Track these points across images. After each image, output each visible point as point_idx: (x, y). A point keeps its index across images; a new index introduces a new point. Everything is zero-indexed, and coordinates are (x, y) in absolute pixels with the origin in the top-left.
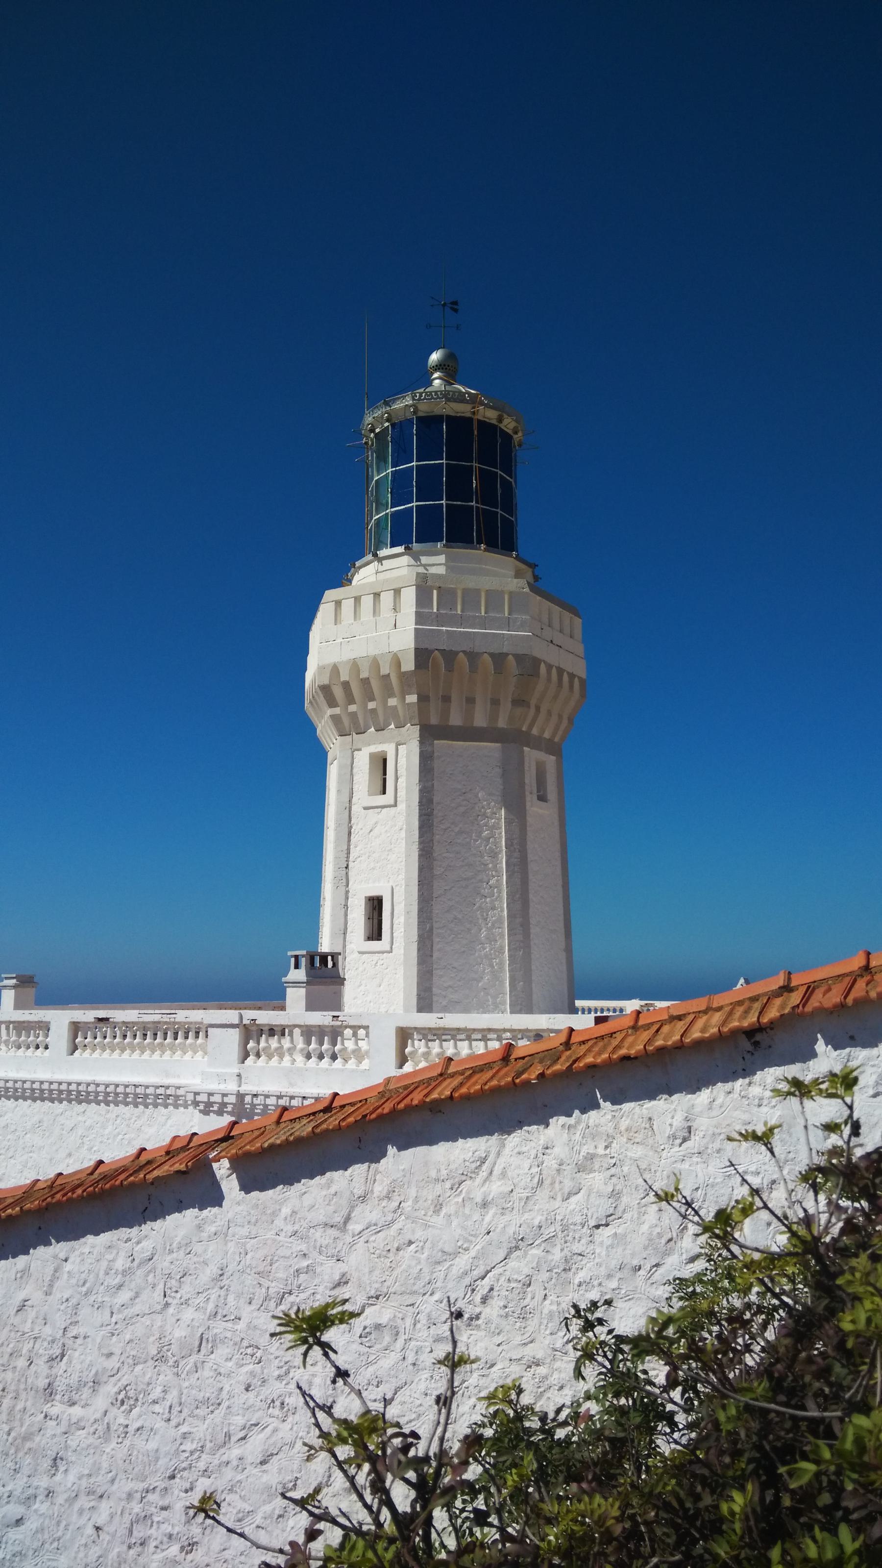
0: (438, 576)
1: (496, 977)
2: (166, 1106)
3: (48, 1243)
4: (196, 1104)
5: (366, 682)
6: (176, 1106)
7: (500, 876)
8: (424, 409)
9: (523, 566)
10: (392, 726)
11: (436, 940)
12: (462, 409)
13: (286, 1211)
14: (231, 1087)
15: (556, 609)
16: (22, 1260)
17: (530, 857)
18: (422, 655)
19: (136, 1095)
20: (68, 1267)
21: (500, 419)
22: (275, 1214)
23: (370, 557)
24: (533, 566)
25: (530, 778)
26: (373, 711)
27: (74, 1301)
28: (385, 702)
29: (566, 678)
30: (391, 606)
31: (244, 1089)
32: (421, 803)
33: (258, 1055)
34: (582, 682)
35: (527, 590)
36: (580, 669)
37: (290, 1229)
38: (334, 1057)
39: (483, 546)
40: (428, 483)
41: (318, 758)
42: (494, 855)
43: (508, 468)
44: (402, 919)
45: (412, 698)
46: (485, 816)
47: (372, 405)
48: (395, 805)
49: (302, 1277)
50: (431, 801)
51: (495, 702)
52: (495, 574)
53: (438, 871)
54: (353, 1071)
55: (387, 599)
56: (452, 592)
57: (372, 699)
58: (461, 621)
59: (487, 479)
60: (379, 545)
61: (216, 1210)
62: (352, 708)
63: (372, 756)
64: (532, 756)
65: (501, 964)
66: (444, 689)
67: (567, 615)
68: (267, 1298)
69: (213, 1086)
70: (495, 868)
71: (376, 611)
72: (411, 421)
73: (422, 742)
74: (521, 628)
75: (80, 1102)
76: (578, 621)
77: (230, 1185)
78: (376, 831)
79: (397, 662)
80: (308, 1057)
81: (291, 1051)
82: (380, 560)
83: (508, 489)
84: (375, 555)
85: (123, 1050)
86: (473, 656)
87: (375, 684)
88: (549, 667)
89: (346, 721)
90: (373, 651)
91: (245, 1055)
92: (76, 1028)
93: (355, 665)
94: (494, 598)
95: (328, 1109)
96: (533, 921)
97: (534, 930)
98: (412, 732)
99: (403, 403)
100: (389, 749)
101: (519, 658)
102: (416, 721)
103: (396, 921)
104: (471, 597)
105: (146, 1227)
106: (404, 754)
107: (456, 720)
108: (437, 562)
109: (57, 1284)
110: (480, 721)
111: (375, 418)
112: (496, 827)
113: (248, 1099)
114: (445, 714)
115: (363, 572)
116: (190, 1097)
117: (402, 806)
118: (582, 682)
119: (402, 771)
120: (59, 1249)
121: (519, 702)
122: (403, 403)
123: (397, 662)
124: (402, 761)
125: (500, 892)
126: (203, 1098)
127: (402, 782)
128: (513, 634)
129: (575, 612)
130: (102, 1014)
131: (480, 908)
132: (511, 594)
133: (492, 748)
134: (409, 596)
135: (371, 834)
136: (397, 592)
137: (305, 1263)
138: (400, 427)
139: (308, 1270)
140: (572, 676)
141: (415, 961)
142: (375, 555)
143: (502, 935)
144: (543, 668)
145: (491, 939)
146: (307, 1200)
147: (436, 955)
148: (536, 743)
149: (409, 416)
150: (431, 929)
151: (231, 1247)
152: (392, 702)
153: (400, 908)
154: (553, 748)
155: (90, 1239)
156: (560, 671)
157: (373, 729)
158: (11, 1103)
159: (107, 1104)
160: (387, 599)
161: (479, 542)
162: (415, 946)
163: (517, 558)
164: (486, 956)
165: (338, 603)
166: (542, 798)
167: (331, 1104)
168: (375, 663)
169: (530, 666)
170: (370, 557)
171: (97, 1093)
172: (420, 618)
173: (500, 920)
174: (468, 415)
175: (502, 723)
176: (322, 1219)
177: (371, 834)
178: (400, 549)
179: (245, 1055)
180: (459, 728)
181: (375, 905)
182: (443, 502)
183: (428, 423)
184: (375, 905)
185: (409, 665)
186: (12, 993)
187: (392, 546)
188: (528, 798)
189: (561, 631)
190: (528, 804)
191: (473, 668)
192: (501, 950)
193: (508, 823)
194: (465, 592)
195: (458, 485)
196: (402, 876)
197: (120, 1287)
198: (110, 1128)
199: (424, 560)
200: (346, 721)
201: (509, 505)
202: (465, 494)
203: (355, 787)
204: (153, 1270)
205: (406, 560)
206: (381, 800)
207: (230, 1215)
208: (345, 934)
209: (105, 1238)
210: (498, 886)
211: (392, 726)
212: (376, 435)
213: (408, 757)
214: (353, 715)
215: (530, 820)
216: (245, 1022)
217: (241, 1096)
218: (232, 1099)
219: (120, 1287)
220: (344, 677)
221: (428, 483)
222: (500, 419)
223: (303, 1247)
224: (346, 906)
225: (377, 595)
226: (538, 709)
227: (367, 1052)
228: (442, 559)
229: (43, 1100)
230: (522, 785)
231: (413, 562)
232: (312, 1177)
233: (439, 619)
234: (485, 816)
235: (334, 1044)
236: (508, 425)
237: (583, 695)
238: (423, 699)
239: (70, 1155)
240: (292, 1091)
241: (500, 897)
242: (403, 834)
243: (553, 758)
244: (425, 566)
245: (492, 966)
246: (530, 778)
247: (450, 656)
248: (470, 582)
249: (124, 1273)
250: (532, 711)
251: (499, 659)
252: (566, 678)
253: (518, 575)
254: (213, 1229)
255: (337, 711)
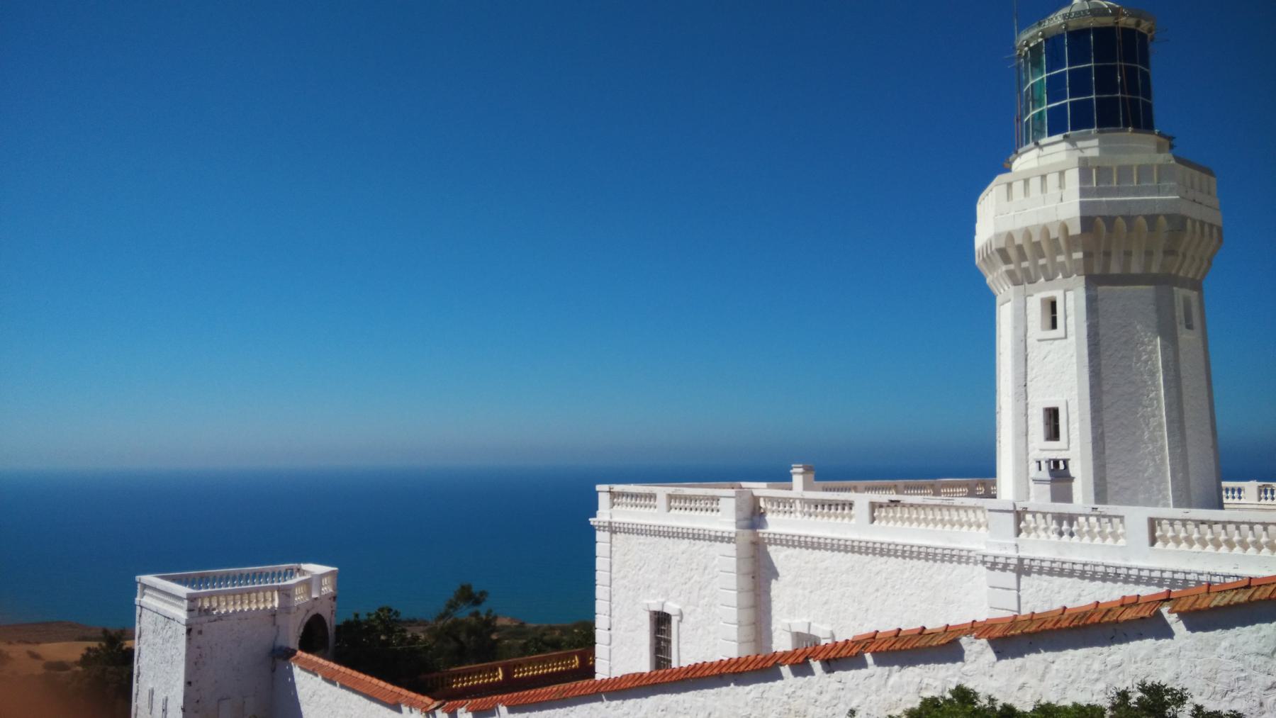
0: (1093, 158)
1: (1159, 469)
2: (951, 562)
3: (1038, 652)
4: (984, 563)
5: (1038, 244)
6: (959, 562)
7: (1158, 390)
8: (1074, 25)
9: (1162, 140)
10: (1060, 276)
11: (1107, 441)
12: (1108, 21)
13: (1224, 644)
14: (1011, 552)
15: (1197, 173)
16: (1019, 661)
17: (1183, 374)
18: (1087, 222)
19: (927, 554)
20: (1055, 666)
21: (1138, 24)
22: (1216, 645)
23: (1032, 145)
24: (1170, 138)
25: (1179, 313)
26: (1044, 266)
27: (1062, 686)
28: (1053, 260)
29: (1207, 229)
30: (1057, 184)
31: (1022, 554)
32: (1089, 336)
33: (1072, 534)
34: (1220, 230)
35: (1173, 162)
36: (1217, 218)
37: (1230, 654)
38: (1072, 534)
39: (1130, 129)
40: (1079, 83)
41: (987, 302)
42: (1153, 374)
43: (1145, 62)
44: (1077, 425)
45: (1078, 255)
46: (1143, 343)
47: (1024, 26)
48: (1066, 337)
49: (1241, 683)
50: (1097, 334)
51: (1149, 254)
52: (1140, 150)
53: (1105, 388)
54: (1211, 554)
55: (1053, 179)
56: (1109, 170)
57: (1042, 256)
58: (1119, 192)
59: (1131, 74)
60: (1041, 134)
61: (1168, 641)
62: (1025, 264)
63: (1043, 301)
64: (1180, 293)
65: (1163, 460)
66: (1105, 249)
67: (1205, 176)
68: (1214, 693)
69: (996, 552)
70: (1154, 384)
71: (1026, 193)
72: (1062, 36)
73: (1087, 288)
74: (1171, 192)
75: (882, 555)
76: (1213, 180)
77: (1178, 627)
78: (1049, 358)
79: (1065, 228)
80: (1061, 534)
81: (1036, 529)
82: (1041, 147)
83: (1146, 77)
84: (1037, 144)
85: (843, 517)
86: (1129, 219)
87: (1045, 246)
88: (1194, 221)
89: (1019, 275)
90: (1043, 220)
91: (1019, 532)
92: (874, 506)
93: (1027, 233)
94: (1144, 171)
95: (1248, 587)
96: (1187, 425)
97: (1188, 432)
98: (1079, 283)
99: (1056, 20)
100: (1058, 295)
101: (1169, 217)
102: (1082, 272)
103: (1071, 427)
104: (1124, 172)
105: (1114, 648)
106: (1073, 300)
107: (1115, 269)
108: (1091, 147)
109: (1047, 676)
110: (1136, 268)
111: (1028, 37)
112: (1154, 351)
113: (1026, 562)
114: (1106, 265)
115: (1025, 157)
116: (980, 558)
117: (1072, 338)
118: (1220, 230)
119: (1071, 310)
120: (1049, 656)
121: (1170, 252)
122: (1056, 20)
123: (1065, 228)
124: (1070, 304)
125: (1159, 402)
126: (990, 559)
127: (1071, 320)
128: (1165, 198)
129: (1209, 172)
130: (895, 497)
131: (1143, 416)
132: (1159, 167)
133: (1146, 290)
134: (1073, 177)
135: (1040, 360)
136: (1062, 173)
137: (1243, 675)
138: (1053, 41)
139: (1245, 678)
140: (1211, 226)
141: (1090, 457)
142: (1037, 144)
143: (1162, 437)
144: (1189, 223)
145: (1153, 440)
146: (1241, 639)
147: (1107, 452)
148: (1183, 283)
149: (1060, 32)
150: (1103, 433)
151: (1183, 662)
152: (1060, 258)
153: (1075, 417)
154: (1196, 285)
155: (1071, 652)
156: (1202, 223)
157: (1042, 280)
158: (829, 553)
159: (904, 557)
160: (1053, 179)
161: (1126, 125)
162: (1090, 447)
163: (1160, 134)
164: (1150, 453)
165: (1009, 185)
166: (1189, 327)
167: (1250, 584)
168: (1045, 230)
169: (1178, 223)
170: (1032, 145)
171: (896, 551)
172: (1083, 192)
173: (1160, 425)
174: (1111, 25)
175: (1155, 269)
176: (1254, 650)
177: (1040, 360)
178: (1059, 137)
179: (1019, 532)
180: (1119, 276)
181: (1052, 415)
182: (1093, 96)
183: (1077, 36)
184: (1052, 415)
185: (1075, 229)
186: (801, 477)
187: (1050, 134)
188: (1179, 327)
189: (1209, 193)
190: (1179, 332)
191: (1130, 228)
192: (1162, 448)
193: (1164, 348)
194: (1120, 169)
195: (1105, 80)
196: (1075, 392)
197: (1097, 680)
198: (907, 574)
199: (1080, 144)
200: (1019, 275)
201: (1147, 92)
202: (1106, 85)
203: (1029, 325)
204: (1123, 672)
205: (1064, 145)
206: (1053, 333)
207: (1181, 644)
208: (1027, 435)
209: (1082, 652)
210: (1158, 399)
211: (1060, 276)
212: (1031, 49)
213: (1076, 300)
214: (1026, 271)
215: (1181, 345)
216: (1018, 509)
217: (1021, 560)
218: (1015, 561)
219: (1097, 680)
220: (1036, 238)
221: (1079, 83)
222: (1138, 24)
223: (1241, 665)
224: (1026, 415)
225: (1044, 177)
226: (1184, 256)
227: (1122, 534)
228: (1095, 142)
229: (853, 552)
230: (1174, 318)
231: (1070, 147)
232: (1244, 625)
233: (1100, 192)
234: (1143, 343)
235: (1071, 525)
236: (1144, 26)
237: (1221, 240)
238: (1088, 255)
239: (877, 590)
240: (1063, 558)
241: (1159, 407)
242: (1074, 360)
243: (1195, 293)
244: (1081, 150)
245: (1154, 460)
246: (1179, 313)
247: (1110, 221)
248: (1125, 160)
249: (1100, 672)
250: (1180, 258)
251: (1152, 219)
252: (1207, 229)
253: (1160, 150)
254: (1168, 651)
255: (1012, 267)
